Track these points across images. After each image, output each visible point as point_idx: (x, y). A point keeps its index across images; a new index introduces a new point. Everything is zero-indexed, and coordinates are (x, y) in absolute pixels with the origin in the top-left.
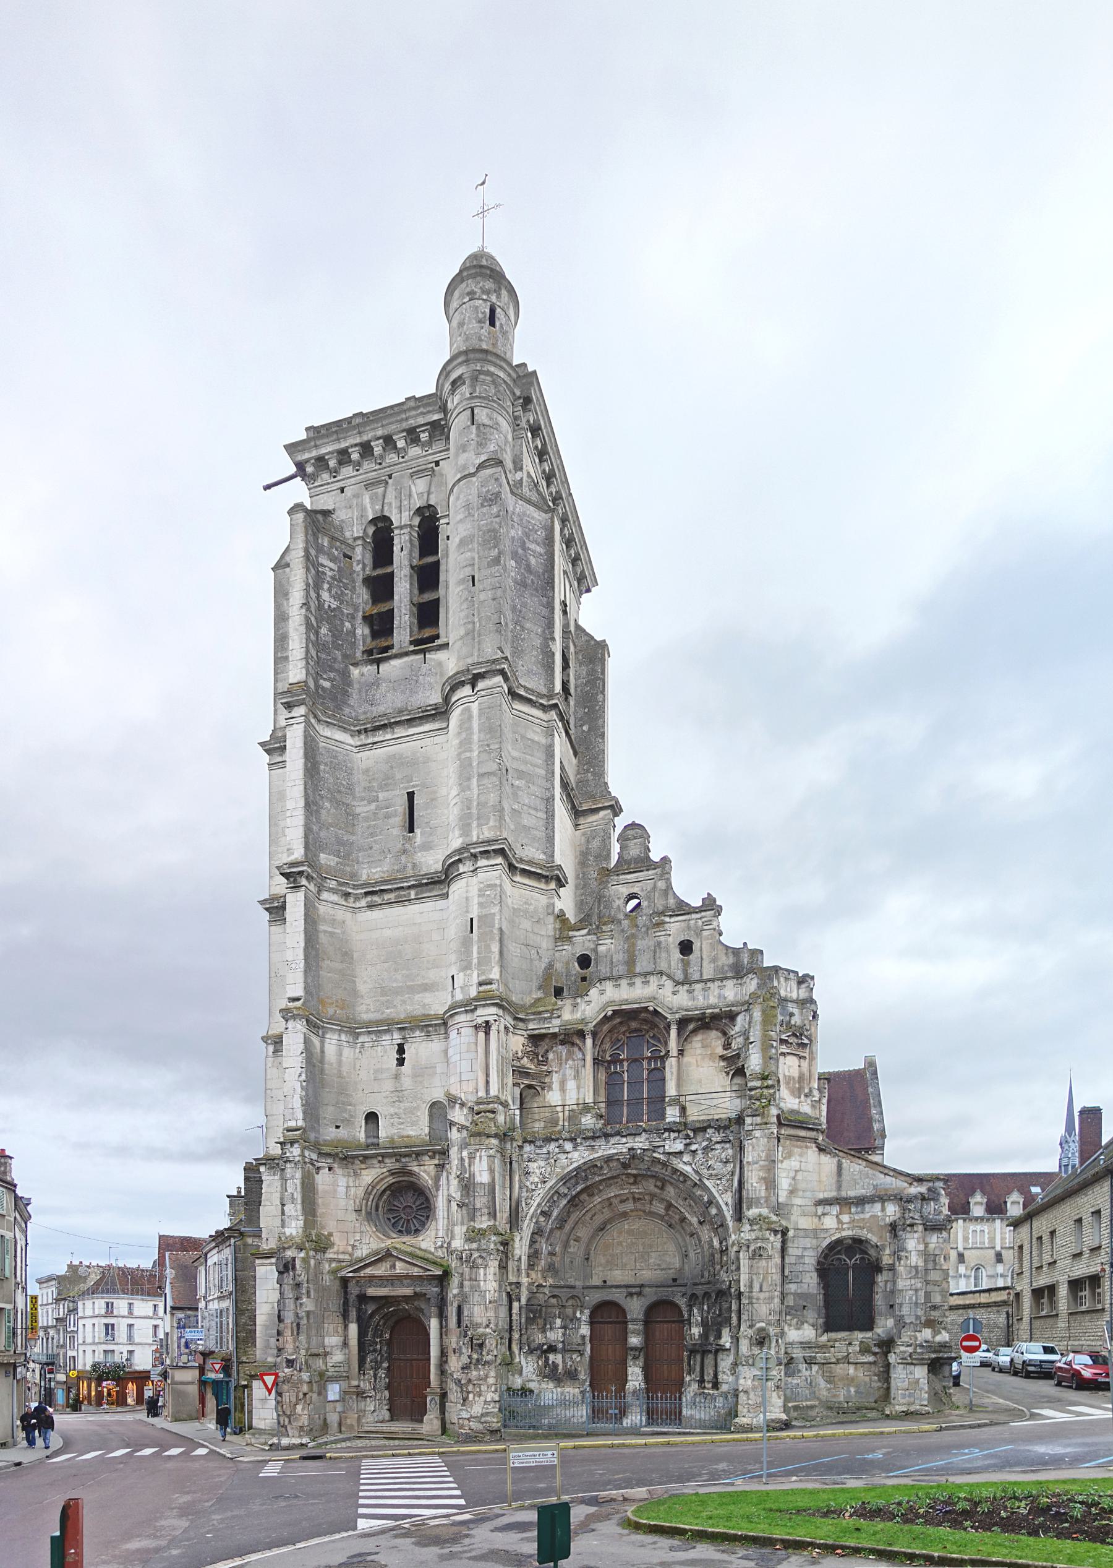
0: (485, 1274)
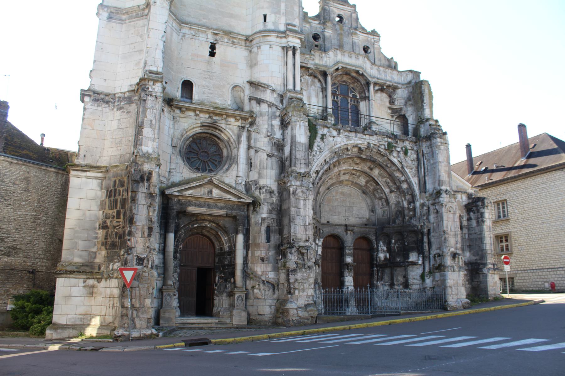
0: (305, 205)
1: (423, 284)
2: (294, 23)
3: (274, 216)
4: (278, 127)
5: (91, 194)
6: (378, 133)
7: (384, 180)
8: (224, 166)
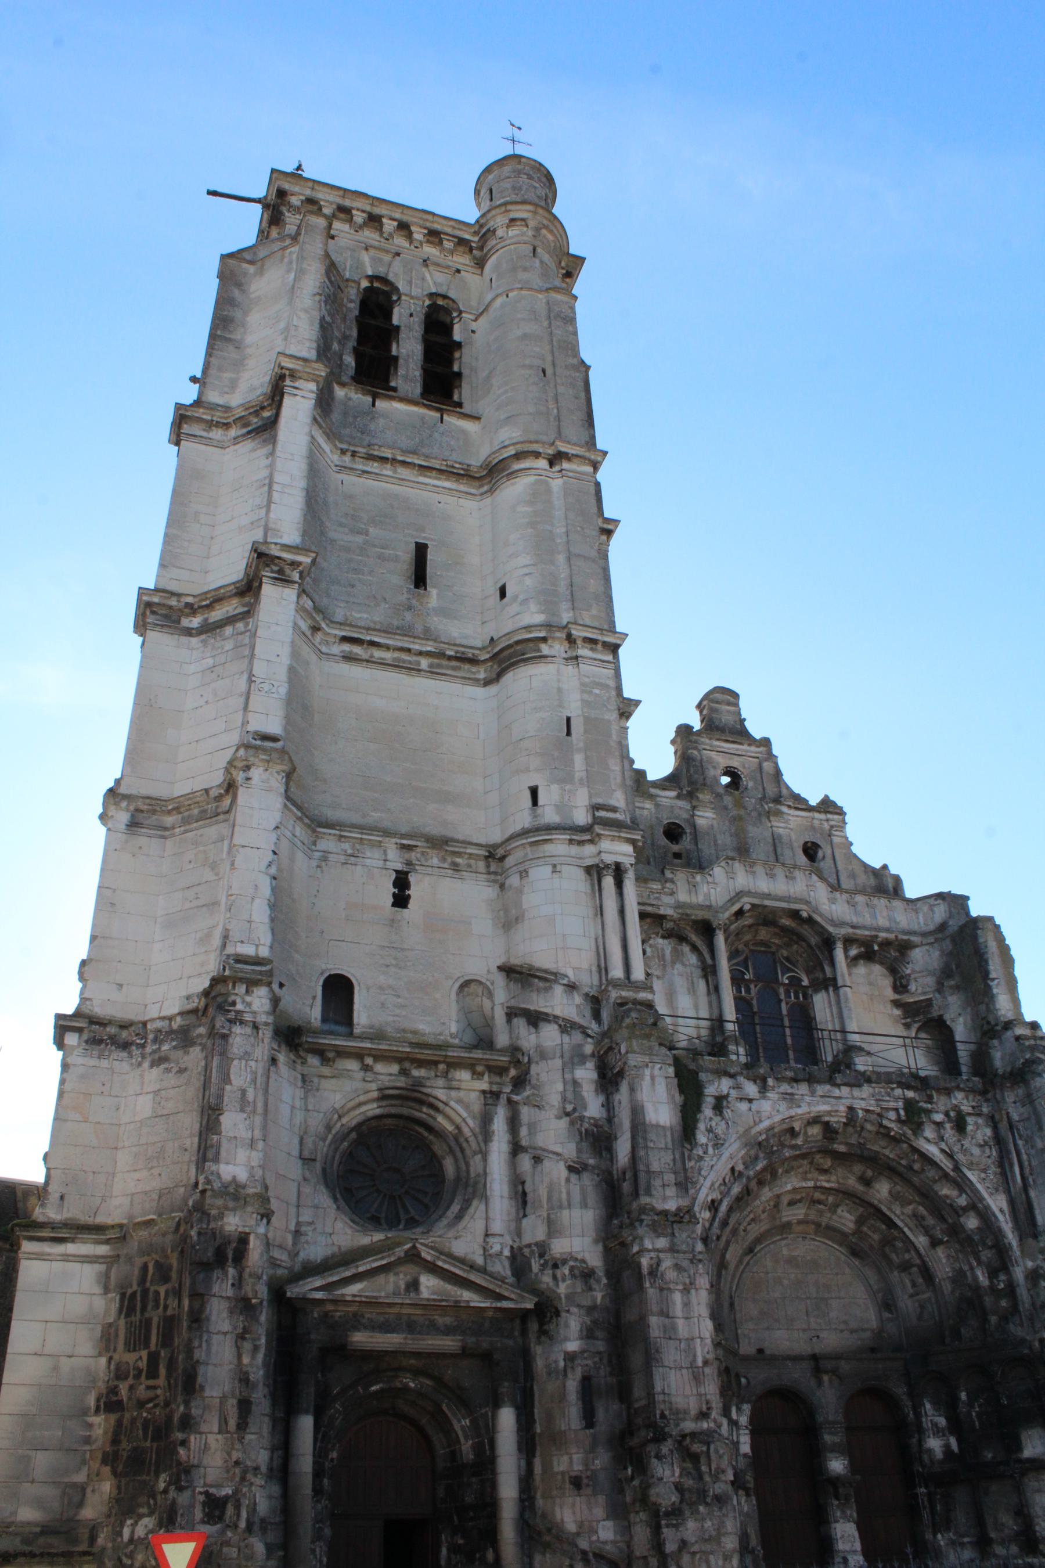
0: (687, 1305)
2: (613, 802)
3: (601, 1346)
4: (592, 1087)
5: (78, 1306)
6: (874, 1077)
7: (909, 1210)
8: (448, 1207)
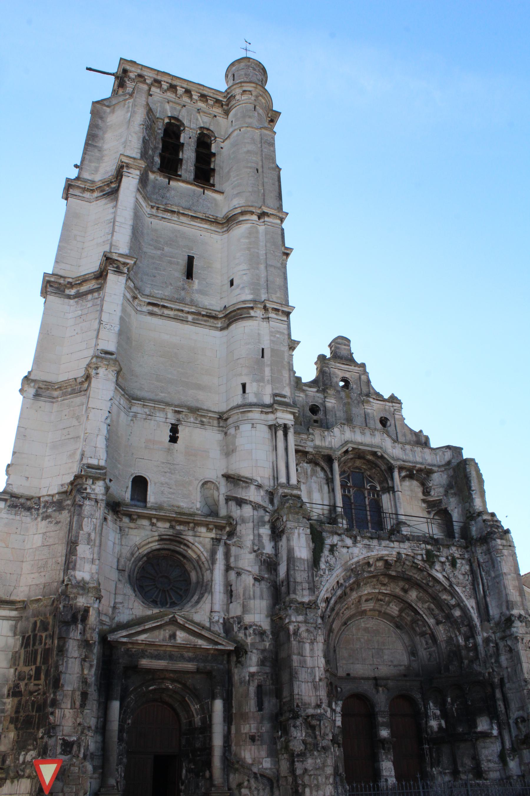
0: (312, 650)
1: (505, 770)
2: (284, 393)
3: (267, 669)
4: (268, 538)
6: (411, 538)
8: (192, 597)
